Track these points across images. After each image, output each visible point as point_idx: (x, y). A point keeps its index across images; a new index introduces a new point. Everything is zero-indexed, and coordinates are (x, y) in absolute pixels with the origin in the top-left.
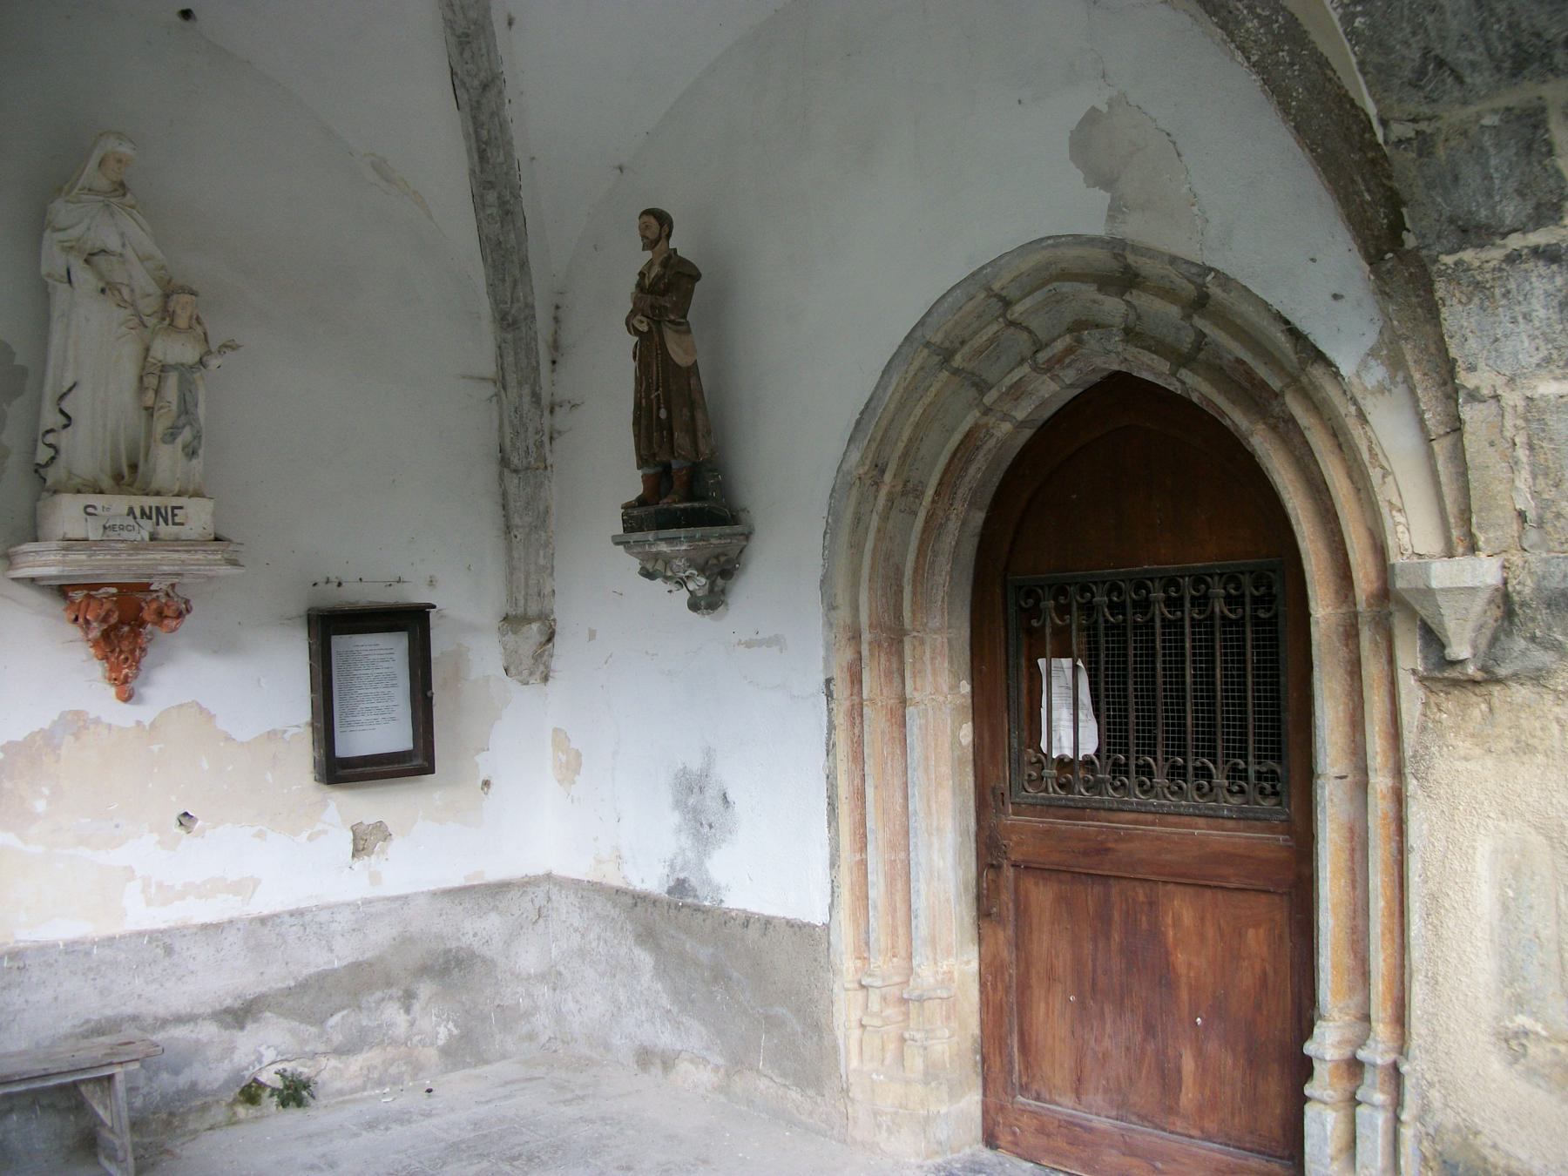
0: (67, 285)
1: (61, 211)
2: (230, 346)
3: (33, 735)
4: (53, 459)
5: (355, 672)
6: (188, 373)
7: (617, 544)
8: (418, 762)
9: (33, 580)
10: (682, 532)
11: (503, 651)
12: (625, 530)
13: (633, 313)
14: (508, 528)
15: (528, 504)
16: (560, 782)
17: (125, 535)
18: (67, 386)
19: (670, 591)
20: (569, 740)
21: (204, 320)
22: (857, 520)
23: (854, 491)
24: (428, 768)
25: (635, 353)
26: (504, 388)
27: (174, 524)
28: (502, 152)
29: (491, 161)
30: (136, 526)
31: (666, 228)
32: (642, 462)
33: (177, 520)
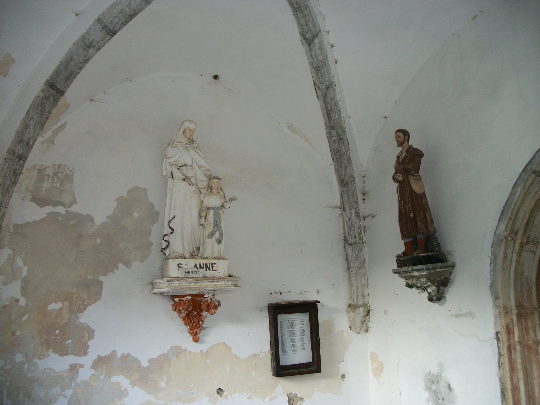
0: (172, 178)
1: (171, 151)
2: (231, 200)
3: (160, 355)
4: (167, 246)
5: (288, 330)
6: (217, 210)
7: (395, 273)
8: (315, 367)
9: (161, 293)
10: (424, 267)
11: (348, 319)
12: (398, 267)
13: (396, 173)
14: (349, 268)
15: (356, 258)
16: (375, 375)
17: (193, 275)
18: (172, 217)
19: (419, 293)
20: (378, 358)
21: (223, 189)
22: (505, 256)
23: (503, 244)
24: (318, 370)
25: (397, 190)
26: (344, 211)
27: (213, 270)
28: (337, 115)
29: (332, 118)
30: (198, 272)
31: (407, 137)
32: (404, 236)
33: (214, 269)
